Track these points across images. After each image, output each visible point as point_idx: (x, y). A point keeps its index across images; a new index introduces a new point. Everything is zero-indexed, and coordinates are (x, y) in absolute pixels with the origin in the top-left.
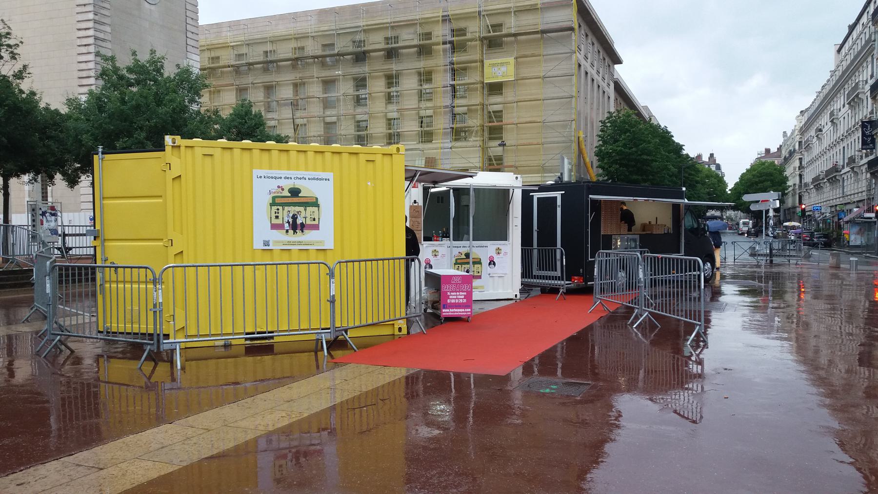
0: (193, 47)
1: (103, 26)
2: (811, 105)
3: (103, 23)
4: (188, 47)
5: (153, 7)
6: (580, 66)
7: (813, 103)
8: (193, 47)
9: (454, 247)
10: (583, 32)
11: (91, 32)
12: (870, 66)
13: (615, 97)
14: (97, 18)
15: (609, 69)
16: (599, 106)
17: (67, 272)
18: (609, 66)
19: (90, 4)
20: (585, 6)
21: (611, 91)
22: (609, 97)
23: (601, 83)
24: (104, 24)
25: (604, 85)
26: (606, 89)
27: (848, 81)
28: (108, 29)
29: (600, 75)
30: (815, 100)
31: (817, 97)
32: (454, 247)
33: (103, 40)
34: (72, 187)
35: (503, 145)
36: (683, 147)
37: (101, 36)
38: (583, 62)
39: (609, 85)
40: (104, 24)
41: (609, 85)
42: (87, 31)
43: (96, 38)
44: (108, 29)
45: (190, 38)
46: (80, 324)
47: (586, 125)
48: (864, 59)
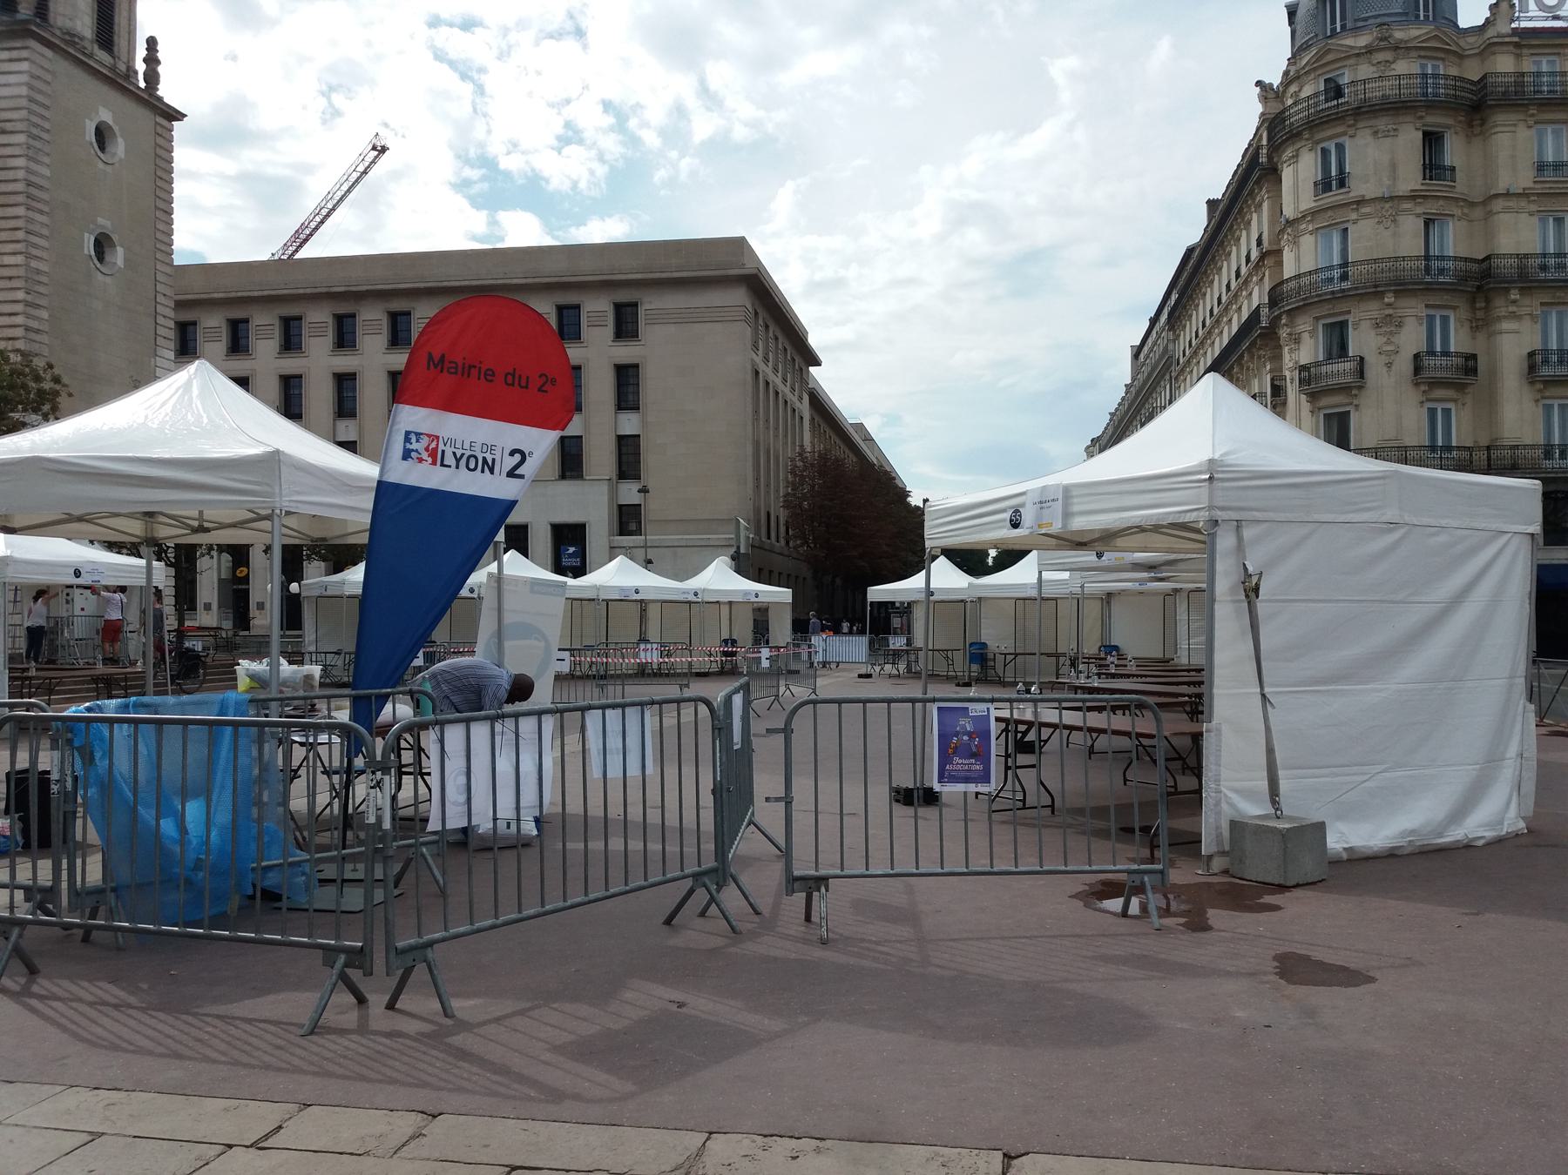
0: (165, 338)
1: (37, 310)
2: (1104, 432)
3: (38, 305)
4: (158, 338)
5: (108, 280)
6: (757, 373)
7: (1106, 428)
8: (165, 338)
9: (1036, 808)
10: (761, 322)
11: (19, 320)
12: (1168, 387)
13: (811, 415)
14: (29, 298)
15: (802, 374)
16: (787, 432)
17: (231, 710)
18: (801, 369)
19: (19, 277)
20: (764, 286)
21: (805, 408)
22: (802, 418)
23: (790, 396)
24: (39, 306)
25: (793, 398)
26: (798, 404)
27: (1160, 382)
28: (45, 314)
29: (788, 384)
30: (1108, 424)
31: (1111, 420)
32: (1036, 808)
33: (38, 331)
34: (1231, 821)
35: (644, 490)
36: (911, 494)
37: (34, 324)
38: (762, 367)
39: (801, 398)
40: (39, 306)
41: (801, 398)
42: (13, 318)
43: (28, 329)
44: (45, 314)
45: (161, 325)
46: (399, 756)
47: (769, 461)
48: (1161, 376)
